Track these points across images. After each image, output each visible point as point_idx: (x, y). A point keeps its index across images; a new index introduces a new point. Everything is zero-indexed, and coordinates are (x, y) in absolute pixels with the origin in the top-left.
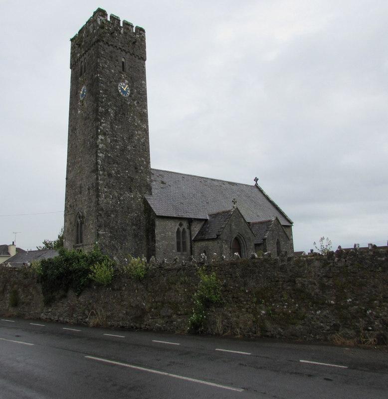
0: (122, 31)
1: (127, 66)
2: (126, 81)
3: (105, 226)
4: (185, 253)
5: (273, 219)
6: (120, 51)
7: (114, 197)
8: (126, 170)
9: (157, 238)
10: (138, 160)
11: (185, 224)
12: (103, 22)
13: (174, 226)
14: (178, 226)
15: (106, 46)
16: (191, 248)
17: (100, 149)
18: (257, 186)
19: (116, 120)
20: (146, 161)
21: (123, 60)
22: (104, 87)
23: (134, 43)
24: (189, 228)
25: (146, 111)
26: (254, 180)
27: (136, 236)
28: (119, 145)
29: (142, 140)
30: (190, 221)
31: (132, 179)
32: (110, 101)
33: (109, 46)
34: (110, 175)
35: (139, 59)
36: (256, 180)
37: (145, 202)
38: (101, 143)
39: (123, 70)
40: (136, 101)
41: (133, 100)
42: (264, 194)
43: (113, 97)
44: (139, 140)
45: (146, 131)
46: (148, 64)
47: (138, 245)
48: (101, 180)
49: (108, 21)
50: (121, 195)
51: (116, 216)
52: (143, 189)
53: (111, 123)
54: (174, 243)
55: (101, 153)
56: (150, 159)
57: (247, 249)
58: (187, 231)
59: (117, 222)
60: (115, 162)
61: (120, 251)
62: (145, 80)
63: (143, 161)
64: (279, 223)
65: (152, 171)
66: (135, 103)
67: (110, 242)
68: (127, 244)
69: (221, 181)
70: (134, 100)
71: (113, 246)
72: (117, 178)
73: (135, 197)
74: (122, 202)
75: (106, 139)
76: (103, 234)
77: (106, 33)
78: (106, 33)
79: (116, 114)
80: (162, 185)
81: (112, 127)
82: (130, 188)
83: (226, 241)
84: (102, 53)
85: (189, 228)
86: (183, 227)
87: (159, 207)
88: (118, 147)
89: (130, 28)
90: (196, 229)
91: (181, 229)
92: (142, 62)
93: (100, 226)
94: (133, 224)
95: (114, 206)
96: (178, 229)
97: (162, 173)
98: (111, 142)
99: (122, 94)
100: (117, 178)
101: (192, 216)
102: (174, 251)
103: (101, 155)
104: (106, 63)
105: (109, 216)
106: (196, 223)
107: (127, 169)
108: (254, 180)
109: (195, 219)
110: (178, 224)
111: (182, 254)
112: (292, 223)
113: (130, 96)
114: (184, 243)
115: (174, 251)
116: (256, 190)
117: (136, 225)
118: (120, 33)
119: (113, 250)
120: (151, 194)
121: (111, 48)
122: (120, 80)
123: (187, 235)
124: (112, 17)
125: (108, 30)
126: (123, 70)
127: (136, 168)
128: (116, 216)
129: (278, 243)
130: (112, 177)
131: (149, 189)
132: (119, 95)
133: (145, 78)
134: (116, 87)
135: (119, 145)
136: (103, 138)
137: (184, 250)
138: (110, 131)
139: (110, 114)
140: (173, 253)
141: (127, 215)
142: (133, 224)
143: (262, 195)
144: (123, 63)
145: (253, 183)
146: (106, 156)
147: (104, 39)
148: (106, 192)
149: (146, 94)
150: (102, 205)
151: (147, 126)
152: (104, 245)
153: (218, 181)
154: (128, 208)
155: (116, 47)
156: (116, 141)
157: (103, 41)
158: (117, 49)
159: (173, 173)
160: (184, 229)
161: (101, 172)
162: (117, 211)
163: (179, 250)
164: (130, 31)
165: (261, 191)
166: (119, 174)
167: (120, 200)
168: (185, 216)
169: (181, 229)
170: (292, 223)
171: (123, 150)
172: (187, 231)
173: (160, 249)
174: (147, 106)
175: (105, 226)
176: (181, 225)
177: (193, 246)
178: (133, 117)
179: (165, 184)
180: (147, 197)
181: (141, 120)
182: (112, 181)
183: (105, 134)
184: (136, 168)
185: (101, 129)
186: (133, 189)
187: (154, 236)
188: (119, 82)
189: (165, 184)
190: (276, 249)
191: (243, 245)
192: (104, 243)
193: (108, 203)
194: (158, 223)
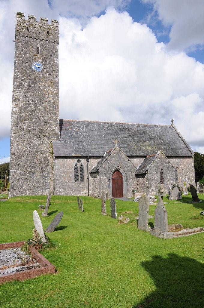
25: (57, 79)
26: (172, 121)
29: (53, 101)
33: (25, 38)
34: (22, 129)
39: (38, 53)
40: (48, 74)
53: (24, 92)
66: (47, 75)
74: (32, 148)
81: (25, 96)
82: (40, 137)
90: (13, 156)
91: (79, 165)
92: (159, 35)
96: (76, 165)
100: (29, 131)
102: (72, 182)
108: (172, 121)
114: (82, 176)
123: (85, 169)
137: (82, 180)
140: (71, 183)
144: (38, 48)
148: (18, 141)
151: (58, 91)
152: (15, 179)
158: (33, 39)
163: (76, 180)
166: (30, 128)
169: (79, 165)
171: (33, 111)
174: (58, 75)
178: (45, 86)
188: (33, 61)
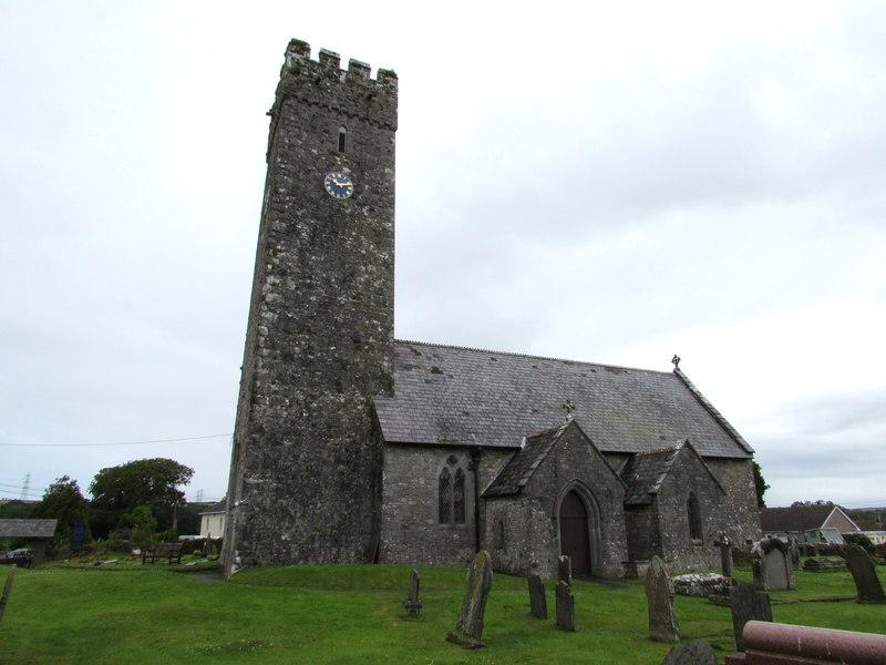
0: (342, 78)
1: (348, 142)
2: (346, 170)
3: (265, 467)
4: (462, 526)
5: (679, 445)
6: (334, 114)
7: (296, 402)
8: (330, 344)
9: (388, 491)
10: (363, 324)
11: (463, 461)
12: (298, 63)
13: (436, 465)
14: (443, 462)
15: (304, 106)
16: (477, 514)
17: (266, 303)
18: (677, 375)
19: (313, 244)
20: (382, 326)
21: (342, 130)
22: (290, 181)
23: (369, 98)
24: (474, 468)
27: (344, 487)
28: (318, 295)
30: (476, 453)
31: (344, 365)
32: (302, 207)
34: (288, 357)
35: (380, 127)
36: (676, 360)
37: (372, 413)
38: (272, 292)
41: (359, 204)
42: (691, 391)
43: (312, 201)
44: (368, 283)
45: (389, 266)
46: (402, 139)
47: (348, 507)
48: (263, 367)
49: (313, 62)
50: (314, 398)
51: (297, 444)
52: (372, 384)
53: (300, 250)
54: (432, 503)
55: (271, 311)
56: (393, 322)
57: (601, 519)
58: (468, 475)
59: (297, 457)
60: (302, 328)
61: (298, 522)
62: (392, 165)
63: (374, 327)
64: (694, 452)
65: (399, 349)
67: (273, 502)
68: (319, 505)
69: (587, 364)
70: (362, 205)
71: (284, 510)
72: (306, 363)
73: (349, 401)
75: (284, 283)
76: (258, 486)
77: (303, 82)
78: (303, 82)
79: (314, 234)
80: (431, 376)
81: (303, 261)
82: (338, 384)
83: (541, 499)
84: (293, 118)
85: (474, 468)
86: (456, 467)
87: (396, 421)
88: (313, 298)
89: (361, 71)
90: (492, 469)
91: (453, 471)
92: (387, 132)
93: (252, 468)
94: (338, 461)
95: (293, 422)
97: (414, 348)
98: (297, 289)
99: (332, 193)
100: (306, 363)
101: (478, 442)
102: (431, 522)
103: (269, 315)
104: (299, 137)
105: (278, 444)
106: (491, 457)
107: (334, 343)
109: (485, 447)
110: (444, 460)
111: (452, 529)
112: (751, 453)
113: (353, 197)
114: (460, 505)
115: (431, 522)
116: (677, 381)
117: (347, 463)
118: (338, 82)
119: (283, 518)
120: (392, 395)
121: (315, 109)
122: (331, 166)
124: (323, 55)
125: (311, 76)
126: (342, 148)
127: (357, 341)
128: (297, 444)
129: (693, 504)
130: (292, 359)
131: (388, 385)
132: (326, 195)
133: (394, 163)
134: (321, 181)
135: (318, 295)
136: (278, 281)
137: (461, 518)
138: (298, 266)
139: (298, 234)
141: (326, 442)
142: (338, 461)
143: (687, 392)
144: (342, 135)
145: (670, 368)
146: (283, 319)
147: (299, 94)
148: (276, 392)
149: (393, 193)
150: (263, 422)
153: (580, 364)
154: (329, 427)
155: (327, 107)
156: (310, 286)
157: (296, 97)
159: (470, 350)
160: (460, 471)
161: (265, 352)
162: (298, 434)
164: (362, 76)
165: (686, 384)
167: (309, 409)
168: (461, 441)
170: (751, 453)
171: (324, 305)
172: (468, 475)
173: (392, 516)
175: (265, 467)
176: (452, 461)
177: (482, 508)
179: (441, 373)
180: (378, 400)
181: (378, 244)
182: (291, 369)
183: (283, 273)
184: (357, 341)
185: (273, 264)
186: (344, 385)
187: (12, 518)
188: (328, 170)
189: (441, 373)
190: (686, 518)
191: (590, 508)
192: (258, 505)
193: (277, 416)
194: (390, 457)
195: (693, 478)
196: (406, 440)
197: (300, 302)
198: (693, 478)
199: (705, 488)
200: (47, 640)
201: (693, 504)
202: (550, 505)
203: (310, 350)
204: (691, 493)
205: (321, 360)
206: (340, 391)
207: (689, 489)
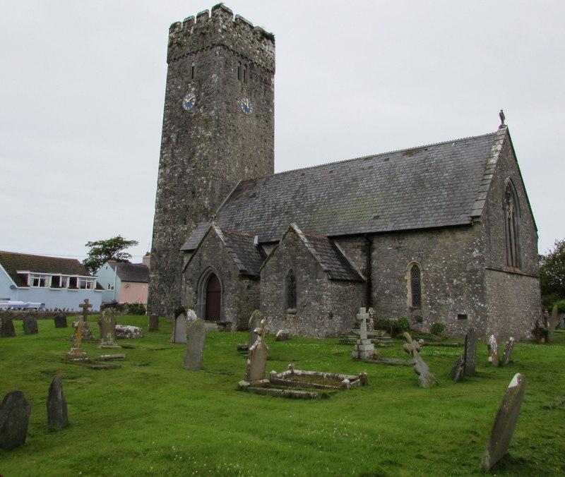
36: (502, 116)
61: (167, 295)
67: (159, 286)
82: (185, 220)
129: (292, 280)
145: (493, 127)
193: (161, 242)
195: (293, 258)
196: (432, 226)
197: (171, 179)
198: (293, 258)
199: (304, 266)
200: (411, 379)
201: (292, 280)
202: (196, 284)
203: (174, 204)
204: (291, 271)
205: (178, 208)
206: (185, 223)
207: (289, 267)
